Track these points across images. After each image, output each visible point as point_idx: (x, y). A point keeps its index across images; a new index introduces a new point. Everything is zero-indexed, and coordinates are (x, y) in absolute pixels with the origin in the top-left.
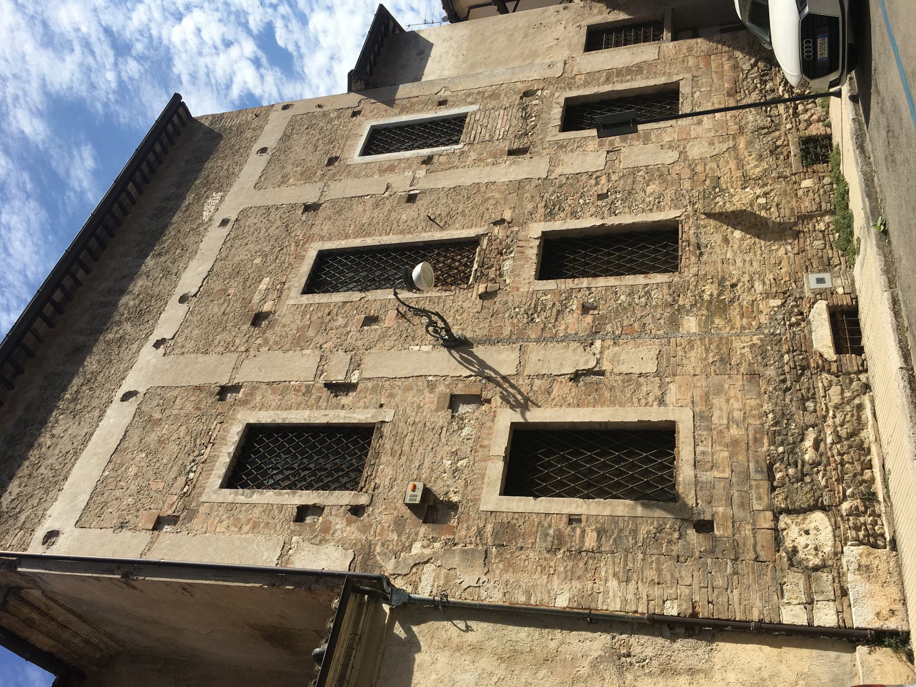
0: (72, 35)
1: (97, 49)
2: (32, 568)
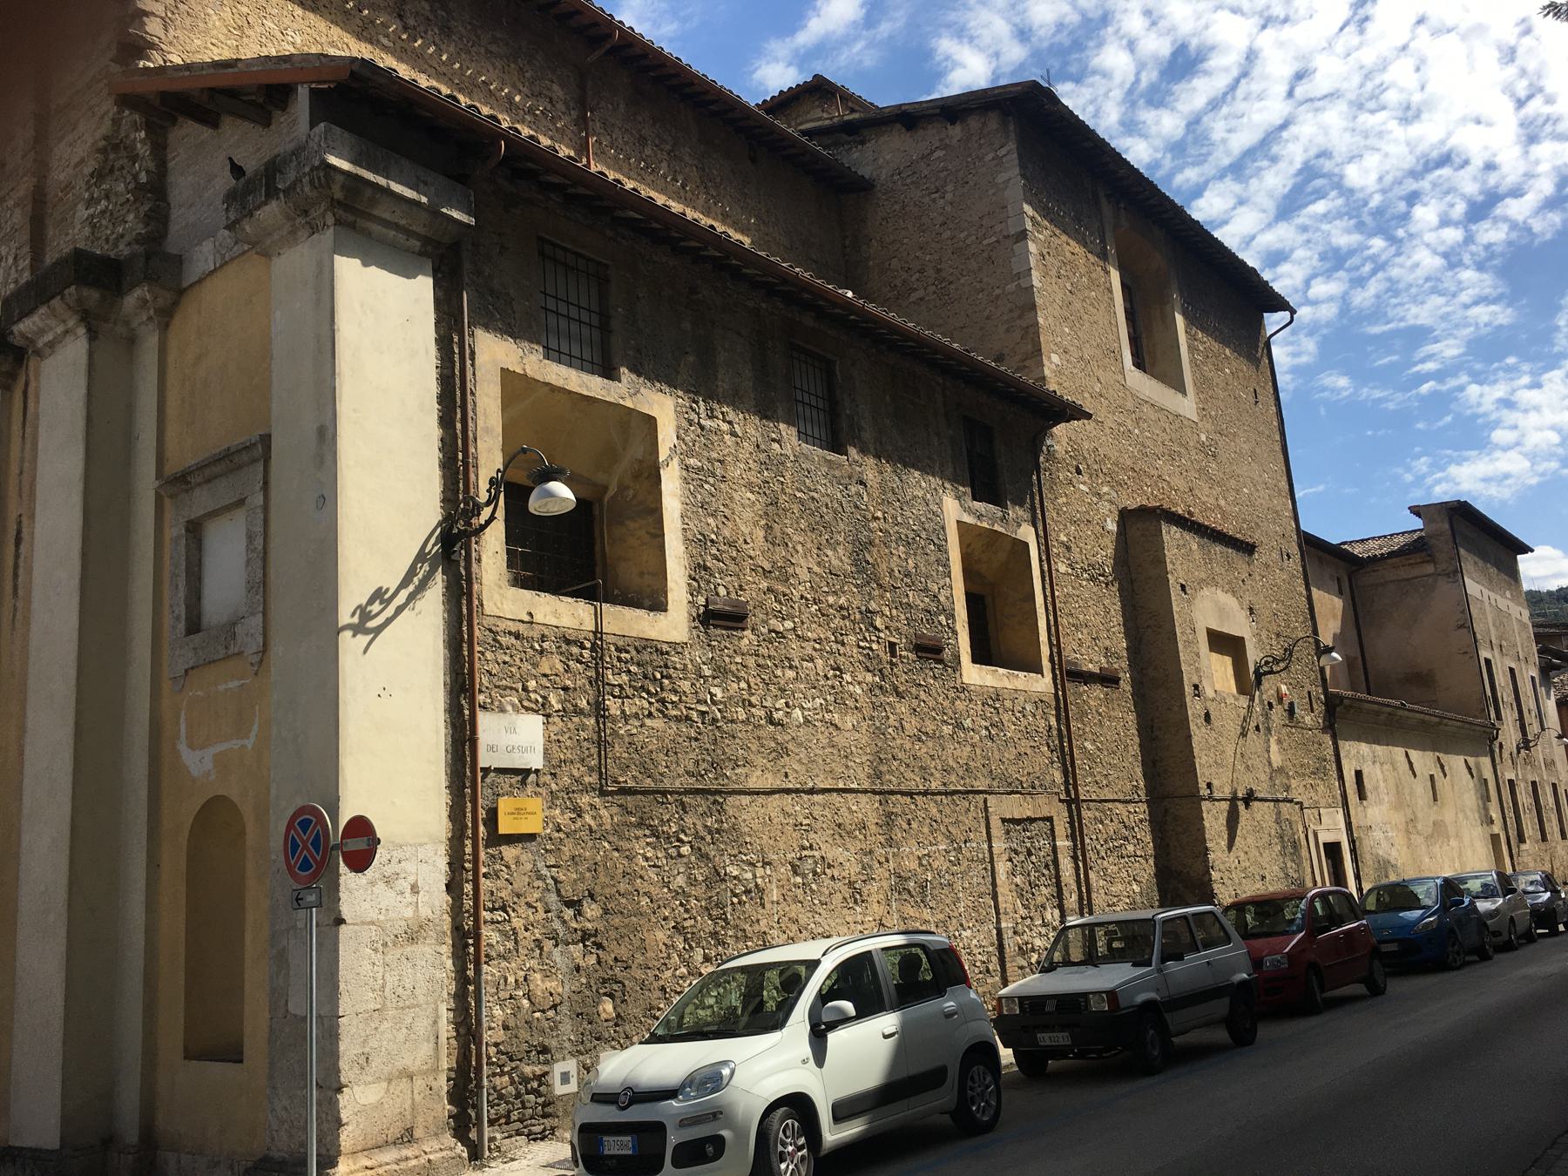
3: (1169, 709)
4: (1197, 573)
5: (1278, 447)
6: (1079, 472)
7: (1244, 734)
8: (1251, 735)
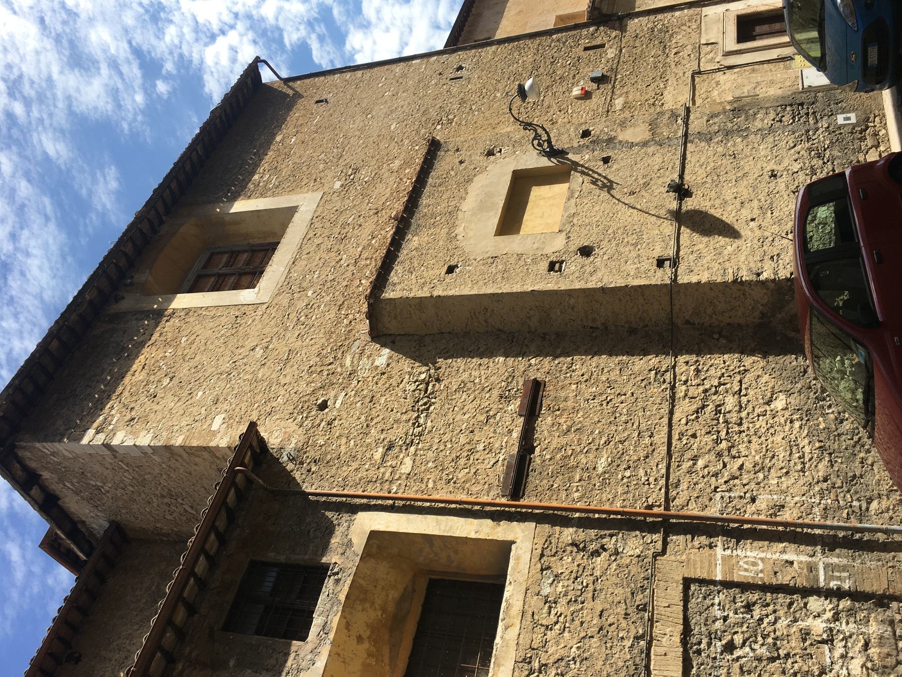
0: (99, 55)
1: (125, 69)
2: (861, 232)
3: (573, 309)
4: (441, 243)
5: (368, 73)
6: (323, 406)
7: (609, 186)
8: (610, 173)
